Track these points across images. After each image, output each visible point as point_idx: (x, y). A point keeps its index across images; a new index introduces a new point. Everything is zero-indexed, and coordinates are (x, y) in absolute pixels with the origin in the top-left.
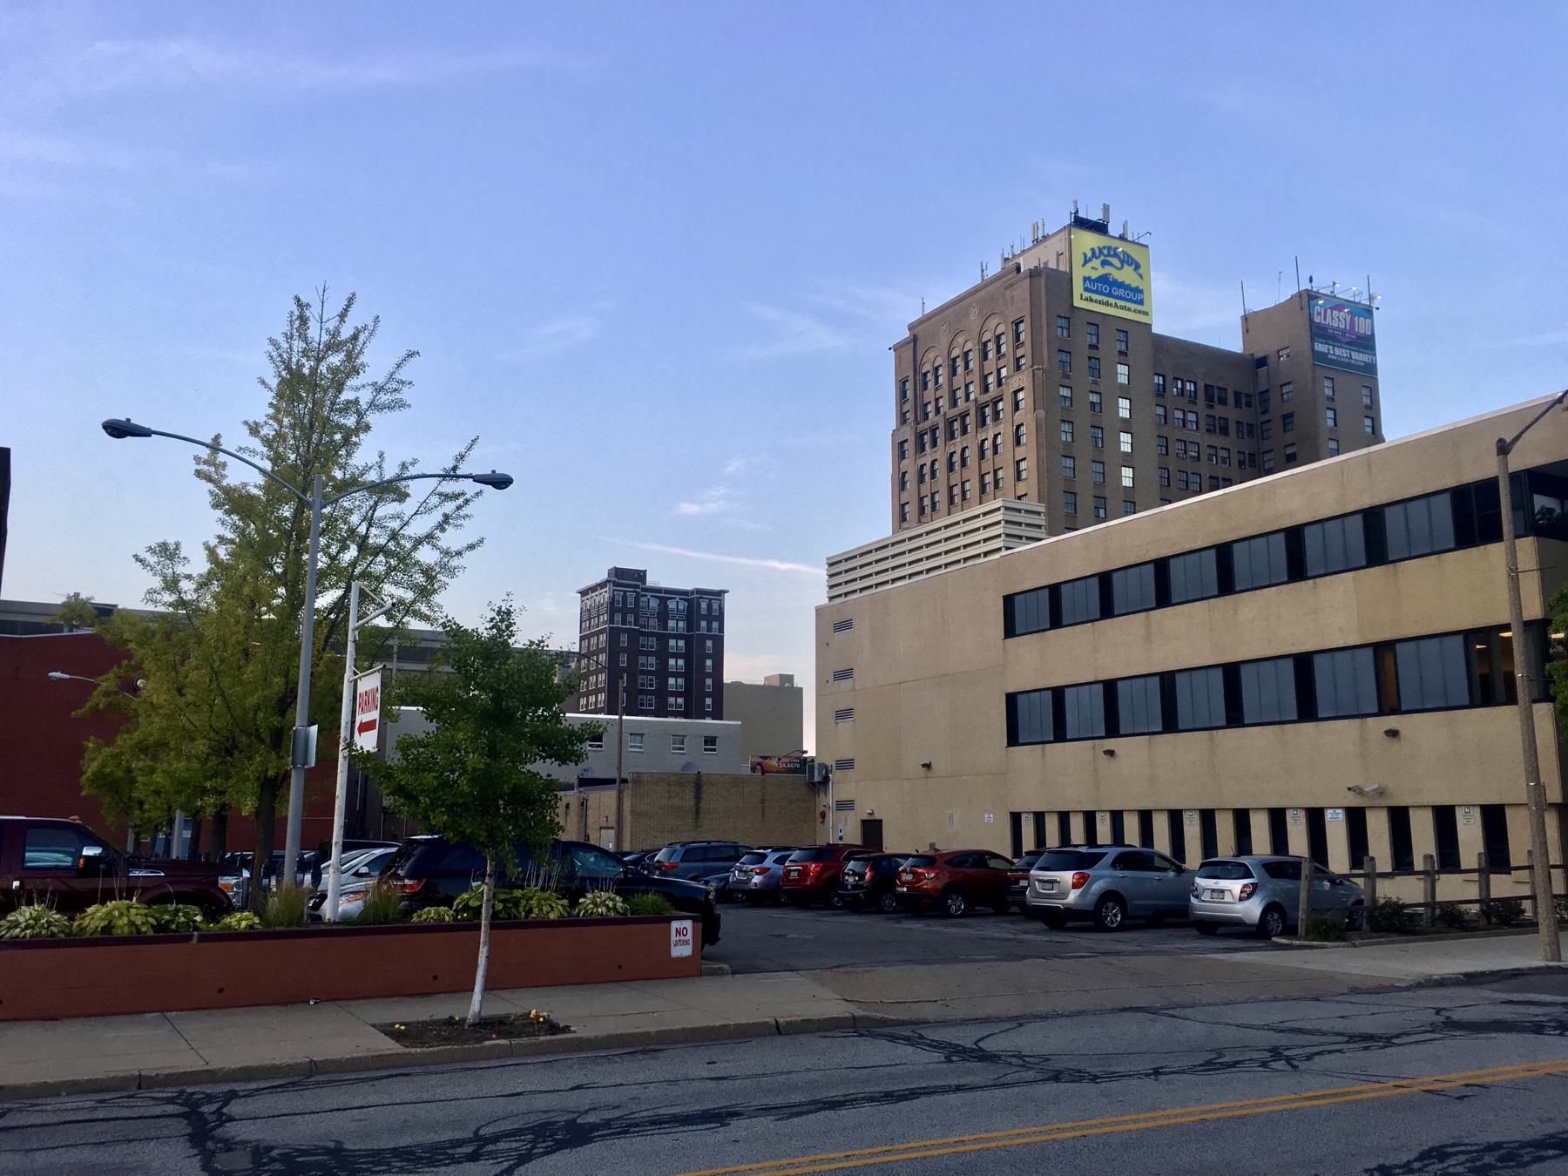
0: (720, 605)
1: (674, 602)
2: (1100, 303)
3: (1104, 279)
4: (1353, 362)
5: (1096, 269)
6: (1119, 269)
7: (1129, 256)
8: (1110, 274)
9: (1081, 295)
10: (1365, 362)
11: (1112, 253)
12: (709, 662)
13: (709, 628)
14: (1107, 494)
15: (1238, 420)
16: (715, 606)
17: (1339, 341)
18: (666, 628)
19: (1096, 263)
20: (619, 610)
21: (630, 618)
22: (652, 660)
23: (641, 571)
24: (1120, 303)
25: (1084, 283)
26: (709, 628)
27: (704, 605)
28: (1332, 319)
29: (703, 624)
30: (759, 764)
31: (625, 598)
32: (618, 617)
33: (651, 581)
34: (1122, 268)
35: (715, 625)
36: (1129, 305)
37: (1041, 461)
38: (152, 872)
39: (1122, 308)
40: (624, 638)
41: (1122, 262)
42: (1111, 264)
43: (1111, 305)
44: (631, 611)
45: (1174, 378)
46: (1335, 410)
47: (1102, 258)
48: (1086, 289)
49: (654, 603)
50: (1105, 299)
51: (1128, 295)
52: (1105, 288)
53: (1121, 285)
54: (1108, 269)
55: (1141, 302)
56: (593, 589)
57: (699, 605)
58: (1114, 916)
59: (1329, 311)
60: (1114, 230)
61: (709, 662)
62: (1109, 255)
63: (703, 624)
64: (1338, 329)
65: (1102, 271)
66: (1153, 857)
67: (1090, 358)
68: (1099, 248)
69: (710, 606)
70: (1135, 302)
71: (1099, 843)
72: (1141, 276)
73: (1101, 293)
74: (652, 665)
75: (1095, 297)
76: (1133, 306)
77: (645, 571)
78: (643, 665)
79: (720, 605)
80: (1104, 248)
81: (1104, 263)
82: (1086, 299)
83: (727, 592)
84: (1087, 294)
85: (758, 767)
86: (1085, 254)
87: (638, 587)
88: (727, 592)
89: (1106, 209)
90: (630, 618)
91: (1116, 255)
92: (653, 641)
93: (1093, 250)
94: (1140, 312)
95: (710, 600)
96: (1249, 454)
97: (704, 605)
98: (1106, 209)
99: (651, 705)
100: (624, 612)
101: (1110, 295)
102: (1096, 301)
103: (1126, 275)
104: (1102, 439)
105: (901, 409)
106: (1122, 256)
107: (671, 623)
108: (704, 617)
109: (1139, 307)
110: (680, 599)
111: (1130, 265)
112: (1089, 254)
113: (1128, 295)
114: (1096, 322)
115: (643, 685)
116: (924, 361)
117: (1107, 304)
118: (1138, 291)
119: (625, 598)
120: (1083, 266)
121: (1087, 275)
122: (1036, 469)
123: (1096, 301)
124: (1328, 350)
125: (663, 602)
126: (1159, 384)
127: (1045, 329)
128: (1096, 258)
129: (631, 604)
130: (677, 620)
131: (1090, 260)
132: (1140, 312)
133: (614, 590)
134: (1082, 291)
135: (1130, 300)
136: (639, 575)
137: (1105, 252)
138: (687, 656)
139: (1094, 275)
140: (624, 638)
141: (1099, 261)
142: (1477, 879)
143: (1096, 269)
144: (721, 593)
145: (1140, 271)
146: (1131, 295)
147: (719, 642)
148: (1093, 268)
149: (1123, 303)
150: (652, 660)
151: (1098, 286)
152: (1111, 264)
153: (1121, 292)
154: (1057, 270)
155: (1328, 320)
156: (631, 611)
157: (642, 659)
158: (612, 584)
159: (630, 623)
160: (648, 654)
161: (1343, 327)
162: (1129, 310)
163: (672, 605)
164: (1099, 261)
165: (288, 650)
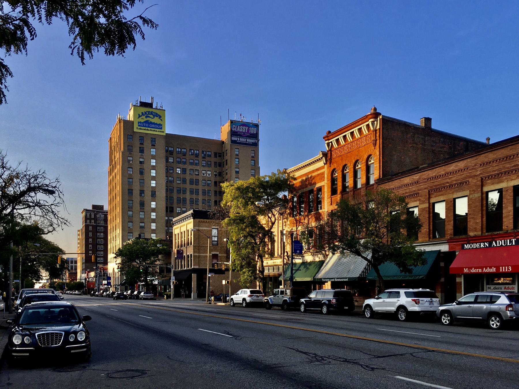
1: (99, 215)
2: (144, 130)
3: (146, 122)
4: (247, 143)
6: (153, 118)
7: (157, 114)
8: (149, 120)
10: (252, 143)
11: (150, 113)
15: (215, 161)
17: (242, 136)
19: (144, 117)
20: (88, 219)
22: (102, 234)
24: (152, 129)
25: (138, 124)
28: (240, 129)
30: (102, 267)
31: (90, 215)
32: (88, 221)
34: (154, 118)
36: (156, 130)
38: (45, 303)
39: (153, 131)
40: (90, 228)
41: (154, 116)
42: (150, 117)
43: (149, 130)
44: (93, 219)
45: (190, 149)
46: (239, 159)
47: (146, 115)
48: (139, 126)
49: (103, 216)
50: (147, 128)
51: (156, 126)
52: (147, 125)
53: (154, 123)
54: (148, 119)
55: (161, 128)
58: (402, 316)
59: (239, 127)
60: (154, 107)
62: (149, 114)
64: (242, 132)
65: (145, 119)
68: (145, 112)
70: (159, 129)
72: (161, 120)
73: (145, 127)
74: (102, 236)
75: (142, 128)
76: (158, 130)
80: (147, 112)
81: (146, 117)
82: (139, 129)
85: (102, 268)
86: (139, 115)
89: (152, 98)
90: (93, 221)
91: (151, 114)
93: (142, 113)
94: (160, 132)
96: (219, 172)
98: (152, 98)
100: (90, 219)
101: (149, 127)
102: (143, 129)
103: (156, 120)
106: (154, 114)
111: (157, 117)
112: (141, 114)
113: (156, 126)
114: (142, 137)
115: (99, 242)
117: (147, 130)
118: (160, 125)
119: (90, 215)
120: (138, 118)
121: (139, 121)
123: (143, 129)
124: (237, 139)
126: (178, 151)
128: (144, 115)
129: (93, 216)
131: (141, 116)
132: (160, 132)
135: (157, 128)
136: (101, 207)
137: (147, 113)
139: (142, 121)
140: (90, 228)
141: (145, 116)
145: (161, 118)
146: (157, 126)
148: (142, 119)
149: (154, 129)
151: (144, 124)
152: (150, 117)
153: (153, 126)
154: (129, 120)
155: (238, 129)
156: (93, 219)
157: (98, 234)
159: (93, 223)
160: (101, 232)
161: (244, 131)
162: (156, 131)
164: (145, 116)
165: (227, 212)
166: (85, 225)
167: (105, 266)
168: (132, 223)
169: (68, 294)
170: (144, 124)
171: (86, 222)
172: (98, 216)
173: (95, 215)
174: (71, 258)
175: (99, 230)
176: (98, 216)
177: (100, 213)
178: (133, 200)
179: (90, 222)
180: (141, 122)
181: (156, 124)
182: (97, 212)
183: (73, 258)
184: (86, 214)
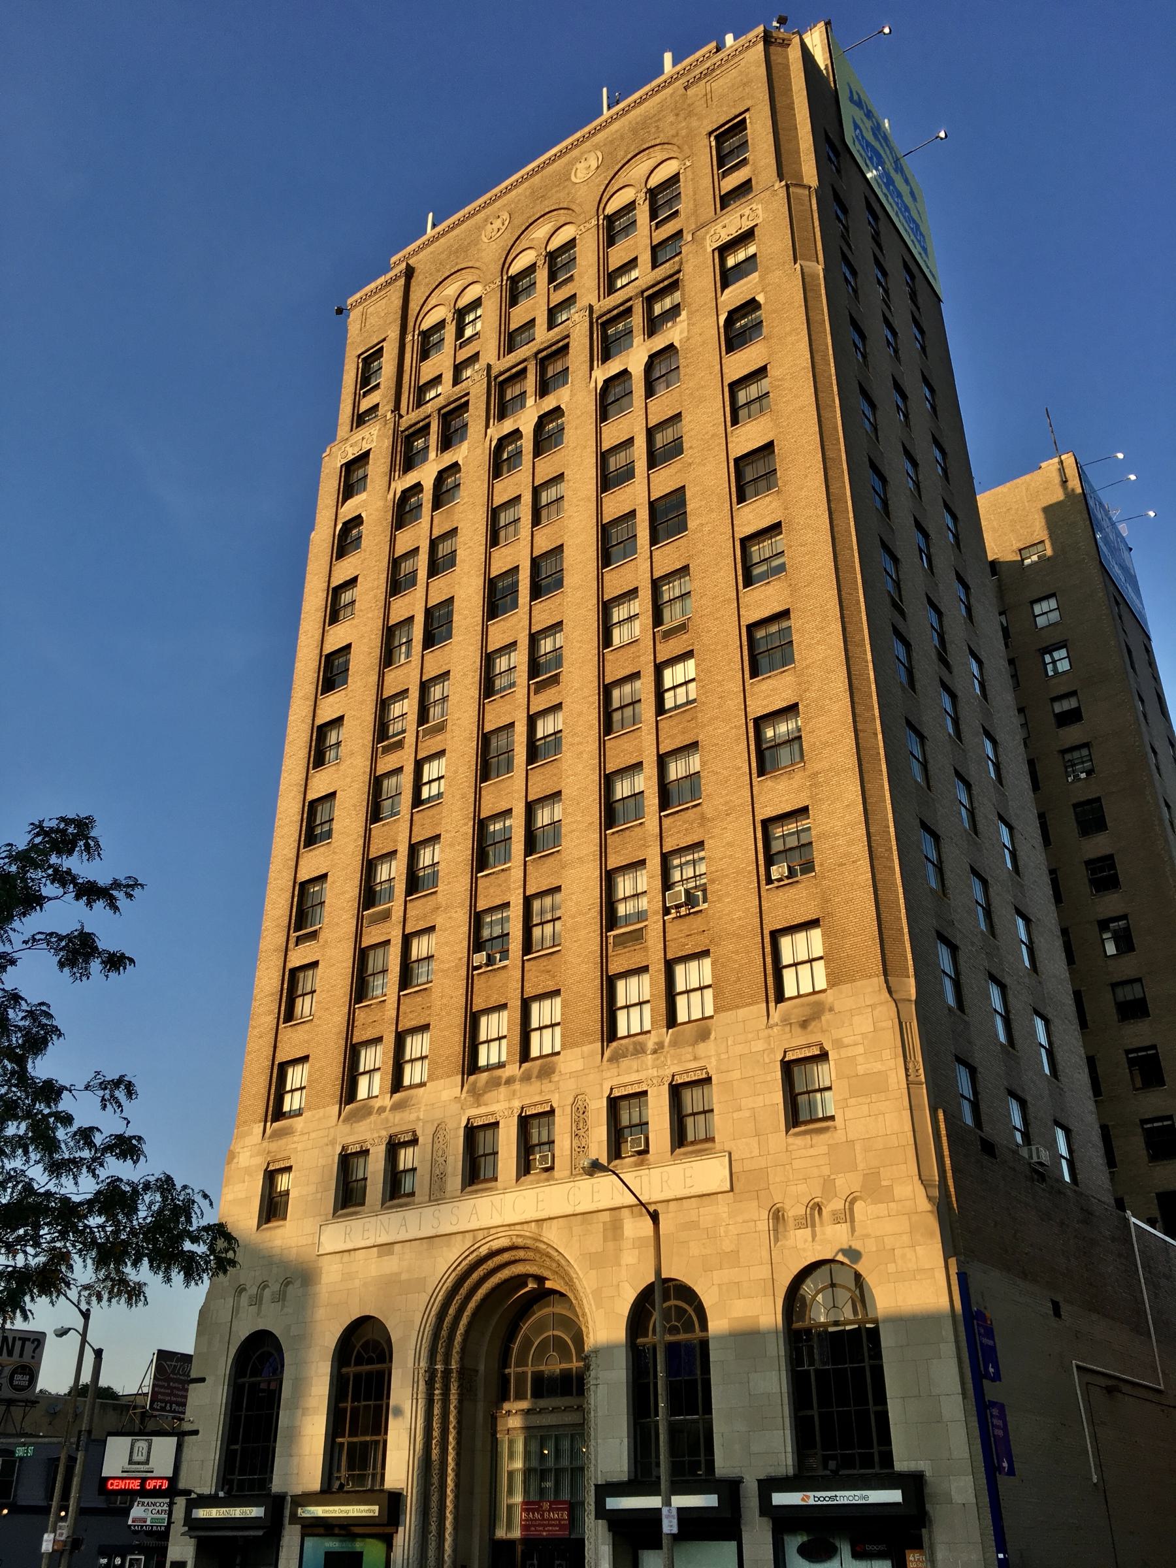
116: (432, 301)
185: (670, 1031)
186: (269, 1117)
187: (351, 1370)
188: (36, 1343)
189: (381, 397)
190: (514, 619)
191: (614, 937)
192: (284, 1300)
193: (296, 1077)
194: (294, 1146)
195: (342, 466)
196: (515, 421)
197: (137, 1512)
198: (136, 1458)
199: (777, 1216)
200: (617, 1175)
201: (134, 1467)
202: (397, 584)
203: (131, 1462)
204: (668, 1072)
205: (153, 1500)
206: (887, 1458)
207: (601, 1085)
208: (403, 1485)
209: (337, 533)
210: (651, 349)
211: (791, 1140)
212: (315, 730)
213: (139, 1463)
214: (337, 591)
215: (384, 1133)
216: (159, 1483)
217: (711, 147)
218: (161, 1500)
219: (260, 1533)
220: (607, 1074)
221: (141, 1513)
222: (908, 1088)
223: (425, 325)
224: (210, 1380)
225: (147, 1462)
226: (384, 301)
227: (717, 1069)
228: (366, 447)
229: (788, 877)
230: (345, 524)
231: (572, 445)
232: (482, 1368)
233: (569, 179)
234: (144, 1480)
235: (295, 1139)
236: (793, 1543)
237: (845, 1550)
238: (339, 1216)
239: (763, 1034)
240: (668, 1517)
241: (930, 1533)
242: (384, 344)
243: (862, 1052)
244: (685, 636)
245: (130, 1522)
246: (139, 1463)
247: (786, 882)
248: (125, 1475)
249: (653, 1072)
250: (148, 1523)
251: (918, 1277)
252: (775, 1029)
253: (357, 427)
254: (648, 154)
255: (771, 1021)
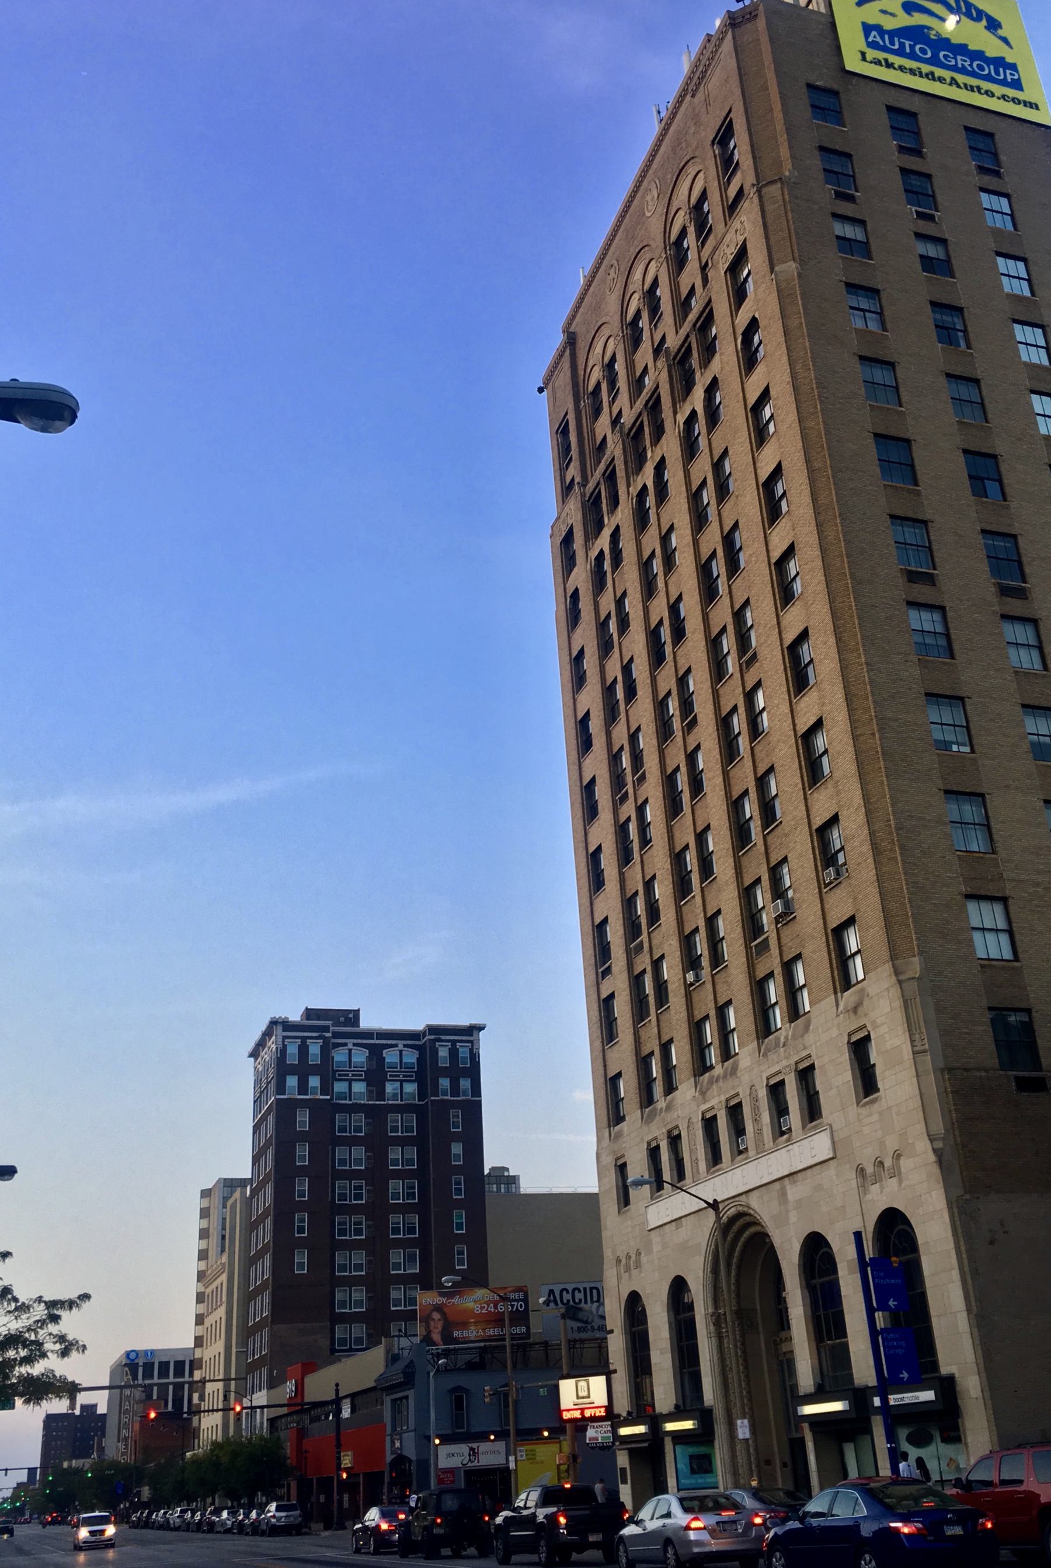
0: (471, 1050)
1: (344, 1051)
5: (893, 15)
8: (930, 28)
9: (863, 54)
12: (457, 1149)
13: (455, 1090)
14: (1001, 446)
16: (463, 1052)
18: (381, 1094)
20: (292, 1070)
21: (314, 1081)
23: (350, 1011)
25: (867, 36)
26: (455, 1090)
27: (443, 1053)
29: (444, 1083)
30: (438, 1308)
31: (303, 1050)
32: (292, 1081)
33: (366, 1023)
35: (465, 1084)
37: (798, 367)
40: (303, 1119)
44: (315, 1070)
48: (873, 45)
54: (918, 19)
56: (261, 1044)
57: (436, 1052)
61: (457, 1149)
63: (444, 1083)
66: (651, 1149)
67: (904, 171)
69: (453, 1053)
70: (1003, 83)
71: (626, 1451)
72: (1005, 40)
73: (912, 56)
74: (358, 1162)
77: (358, 1010)
78: (343, 1162)
79: (471, 1050)
83: (481, 1028)
84: (871, 54)
85: (436, 1316)
87: (326, 1029)
88: (481, 1028)
90: (314, 1081)
92: (360, 1119)
94: (1016, 101)
95: (454, 1042)
97: (443, 1053)
99: (358, 1232)
100: (303, 1071)
104: (965, 331)
105: (562, 479)
107: (390, 1088)
108: (444, 1072)
109: (1011, 93)
110: (405, 1046)
115: (343, 1197)
116: (590, 364)
119: (303, 1050)
122: (790, 389)
125: (375, 1052)
127: (777, 107)
130: (402, 1082)
133: (284, 1038)
134: (862, 45)
138: (420, 1141)
142: (564, 1413)
143: (893, 15)
144: (473, 1030)
147: (473, 1112)
149: (974, 82)
150: (359, 1152)
157: (340, 1152)
158: (280, 1028)
163: (390, 1057)
166: (277, 1100)
167: (456, 1300)
168: (1030, 630)
169: (165, 1526)
170: (902, 45)
171: (281, 1088)
172: (339, 1056)
173: (326, 1050)
174: (146, 1352)
175: (343, 1129)
176: (339, 1056)
177: (350, 1042)
178: (925, 523)
179: (303, 1088)
180: (878, 28)
181: (978, 55)
182: (336, 1035)
183: (153, 1352)
184: (285, 1047)
185: (793, 1024)
186: (838, 990)
187: (817, 1281)
188: (577, 1301)
189: (744, 177)
190: (667, 667)
191: (755, 946)
192: (640, 1267)
193: (852, 941)
194: (624, 1145)
195: (725, 273)
196: (642, 476)
197: (590, 1433)
198: (581, 1394)
199: (861, 1171)
200: (685, 1191)
201: (581, 1401)
202: (699, 519)
203: (578, 1397)
204: (792, 1061)
205: (600, 1424)
206: (934, 1366)
207: (761, 1076)
208: (713, 1404)
209: (739, 347)
210: (704, 384)
211: (860, 1110)
212: (773, 568)
213: (583, 1398)
214: (757, 408)
215: (664, 1130)
216: (597, 1410)
217: (715, 157)
218: (605, 1423)
219: (646, 1445)
220: (763, 1067)
221: (594, 1433)
222: (914, 1058)
223: (591, 388)
224: (616, 1331)
225: (589, 1397)
226: (562, 373)
227: (817, 1055)
228: (741, 239)
229: (835, 879)
230: (743, 334)
231: (674, 493)
232: (758, 1307)
233: (644, 214)
234: (582, 1410)
235: (625, 1139)
236: (903, 1433)
237: (938, 1438)
238: (810, 1130)
239: (836, 1022)
240: (741, 1427)
241: (963, 1422)
242: (731, 115)
243: (887, 1030)
244: (757, 664)
245: (588, 1441)
246: (583, 1398)
247: (836, 882)
248: (576, 1407)
249: (785, 1063)
250: (600, 1441)
251: (935, 1217)
252: (842, 1016)
253: (730, 218)
254: (686, 172)
255: (839, 1010)
